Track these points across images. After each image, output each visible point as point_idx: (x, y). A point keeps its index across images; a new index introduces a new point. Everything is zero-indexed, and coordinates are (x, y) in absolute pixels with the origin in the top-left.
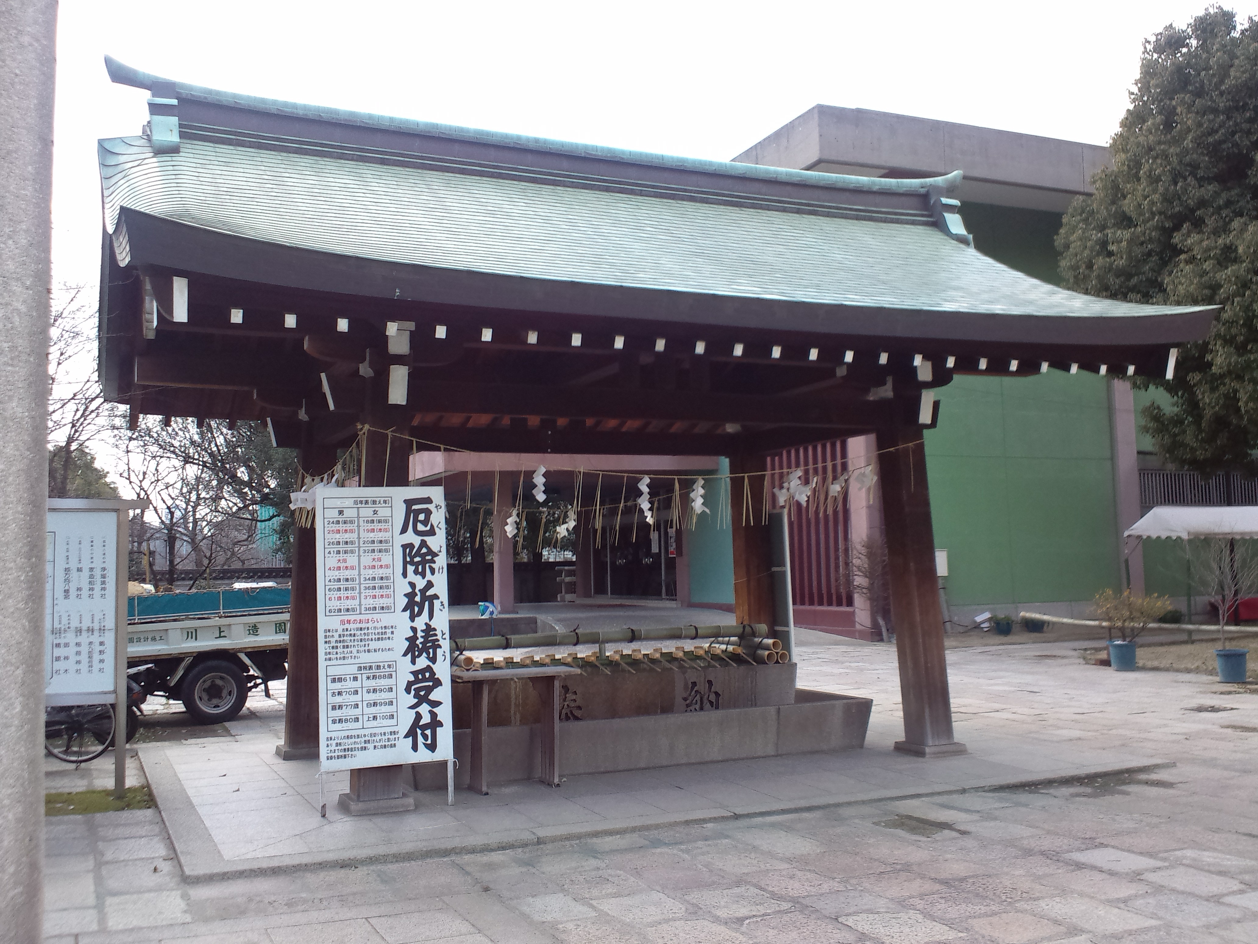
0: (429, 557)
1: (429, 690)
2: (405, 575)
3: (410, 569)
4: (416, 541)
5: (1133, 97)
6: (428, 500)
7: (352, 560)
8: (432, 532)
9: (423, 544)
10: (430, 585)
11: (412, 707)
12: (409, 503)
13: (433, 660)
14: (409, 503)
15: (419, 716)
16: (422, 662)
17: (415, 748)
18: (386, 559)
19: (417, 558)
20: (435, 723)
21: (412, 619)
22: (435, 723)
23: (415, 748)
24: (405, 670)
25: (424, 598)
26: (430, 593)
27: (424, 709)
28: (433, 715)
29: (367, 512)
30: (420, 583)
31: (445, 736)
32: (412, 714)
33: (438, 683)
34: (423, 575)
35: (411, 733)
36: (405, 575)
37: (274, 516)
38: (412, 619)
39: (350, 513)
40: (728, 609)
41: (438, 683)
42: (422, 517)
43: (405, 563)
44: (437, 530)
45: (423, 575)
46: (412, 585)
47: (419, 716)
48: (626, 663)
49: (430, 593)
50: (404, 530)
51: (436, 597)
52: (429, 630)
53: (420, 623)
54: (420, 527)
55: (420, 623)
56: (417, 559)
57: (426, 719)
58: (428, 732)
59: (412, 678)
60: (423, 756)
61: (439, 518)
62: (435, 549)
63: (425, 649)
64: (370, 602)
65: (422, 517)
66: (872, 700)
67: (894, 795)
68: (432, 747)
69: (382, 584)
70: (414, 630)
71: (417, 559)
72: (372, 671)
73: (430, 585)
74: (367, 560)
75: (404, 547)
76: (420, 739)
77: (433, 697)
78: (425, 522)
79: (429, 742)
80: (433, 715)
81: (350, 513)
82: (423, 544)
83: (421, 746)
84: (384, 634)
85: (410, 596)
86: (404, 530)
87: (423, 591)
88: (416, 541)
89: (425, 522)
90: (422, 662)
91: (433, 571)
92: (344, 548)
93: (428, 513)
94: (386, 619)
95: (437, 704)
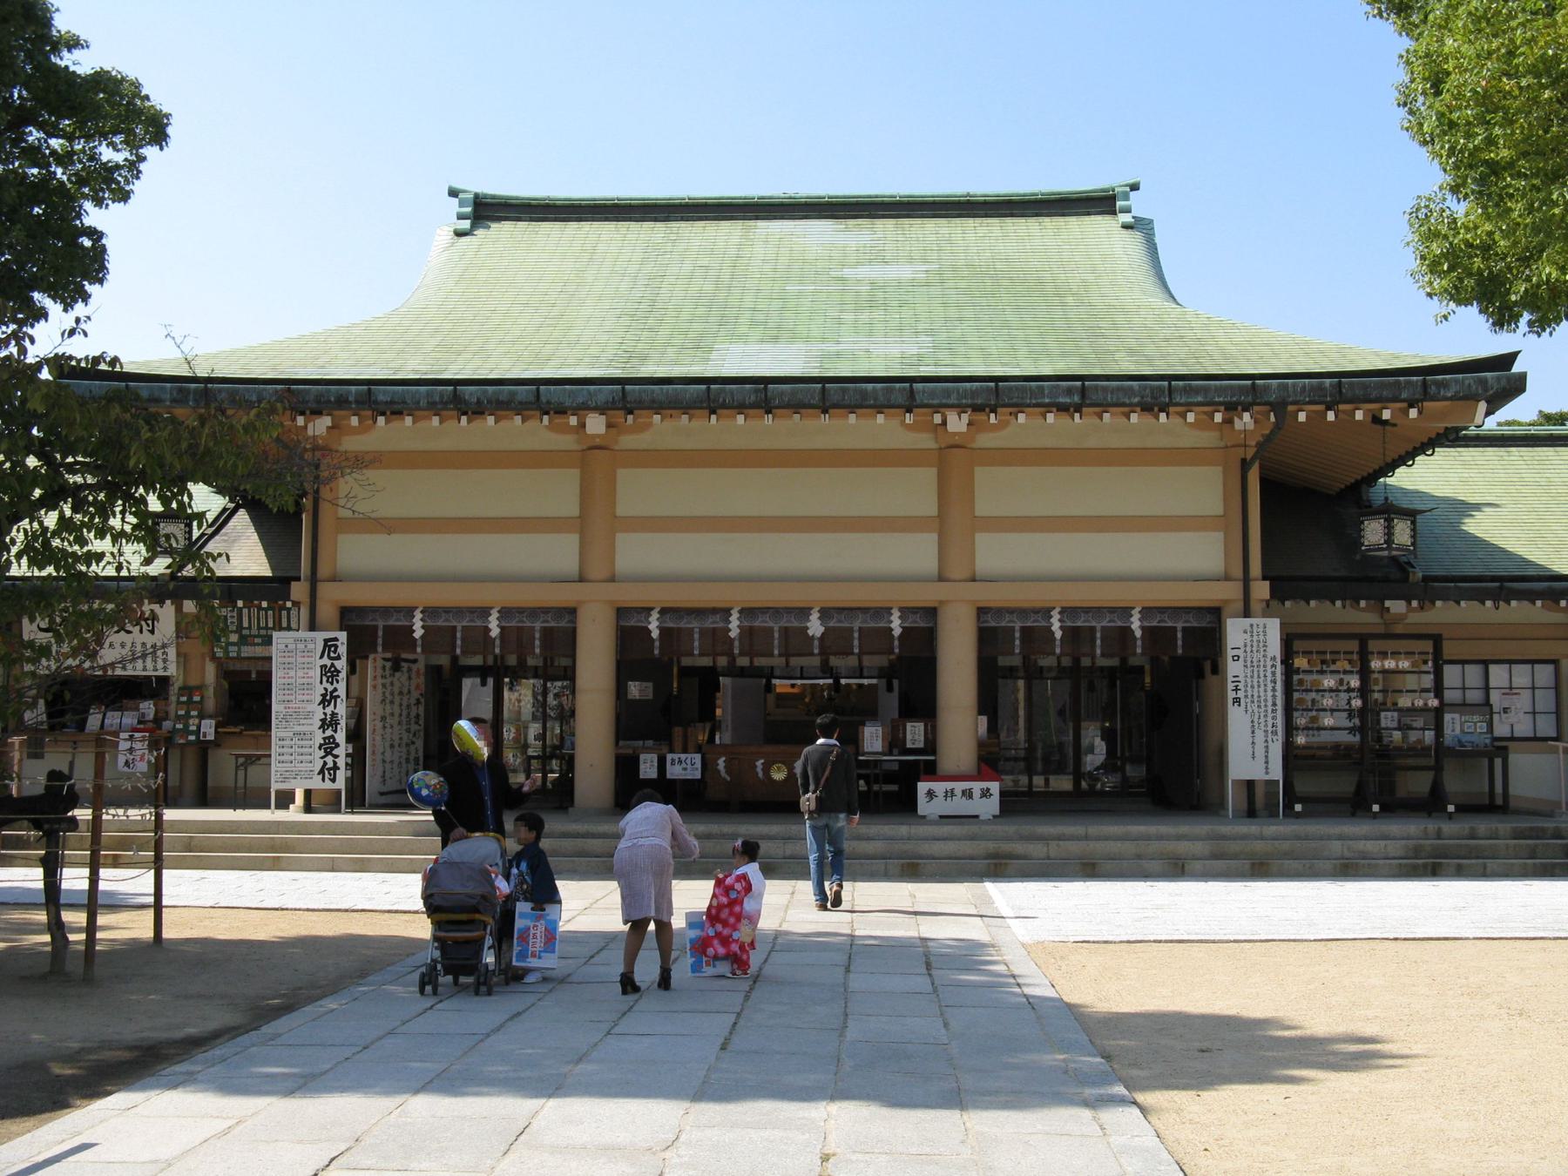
4: (328, 663)
5: (1436, 248)
6: (336, 639)
7: (292, 673)
8: (338, 658)
12: (326, 641)
14: (326, 641)
16: (329, 733)
18: (311, 673)
20: (335, 768)
24: (319, 738)
27: (329, 759)
29: (301, 646)
30: (330, 688)
31: (342, 775)
32: (321, 763)
33: (337, 745)
35: (321, 772)
37: (1008, 759)
39: (291, 647)
40: (556, 854)
41: (337, 745)
52: (333, 714)
53: (329, 710)
55: (329, 710)
57: (330, 764)
60: (328, 785)
61: (342, 650)
63: (330, 725)
64: (300, 697)
66: (101, 281)
68: (333, 780)
69: (309, 687)
72: (301, 735)
74: (300, 673)
81: (291, 647)
84: (309, 715)
85: (324, 696)
88: (328, 663)
90: (329, 733)
92: (287, 666)
94: (310, 707)
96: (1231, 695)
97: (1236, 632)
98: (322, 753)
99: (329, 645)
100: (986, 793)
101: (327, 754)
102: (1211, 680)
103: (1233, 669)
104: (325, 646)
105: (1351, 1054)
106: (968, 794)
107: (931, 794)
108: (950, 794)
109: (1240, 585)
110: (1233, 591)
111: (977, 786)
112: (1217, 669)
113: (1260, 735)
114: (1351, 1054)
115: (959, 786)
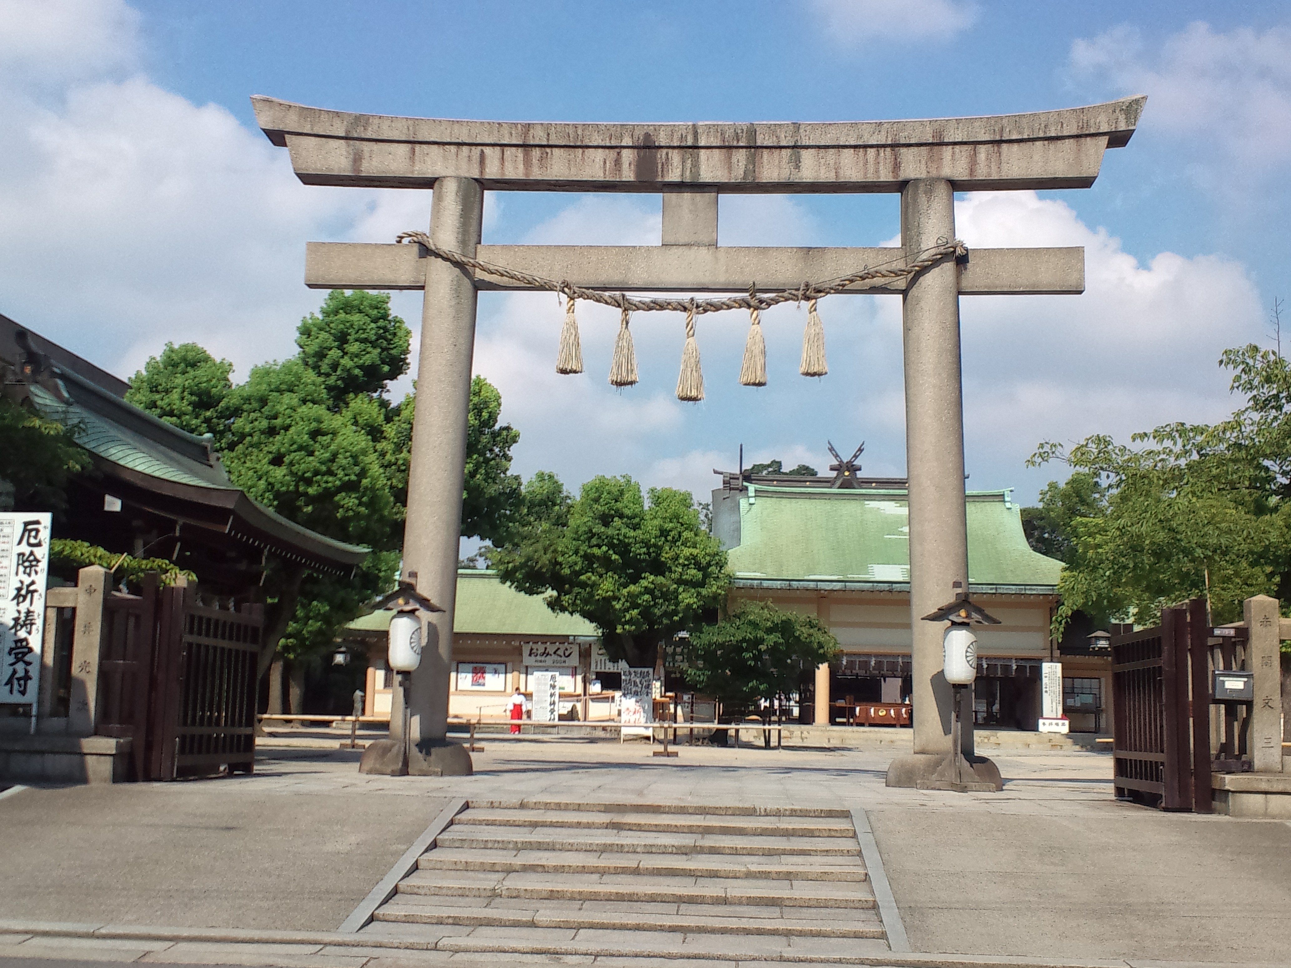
0: (34, 563)
1: (25, 654)
2: (17, 574)
3: (21, 569)
4: (26, 550)
6: (37, 522)
8: (39, 545)
9: (32, 553)
10: (33, 583)
11: (12, 664)
12: (26, 524)
13: (29, 633)
14: (26, 524)
15: (15, 672)
17: (11, 692)
18: (5, 562)
19: (27, 562)
20: (27, 678)
21: (18, 604)
22: (27, 678)
23: (11, 692)
25: (28, 592)
26: (32, 588)
27: (20, 667)
28: (27, 671)
32: (10, 671)
34: (29, 575)
35: (9, 682)
36: (17, 574)
38: (18, 604)
42: (33, 533)
43: (18, 565)
44: (43, 543)
45: (29, 575)
46: (22, 582)
47: (15, 672)
48: (839, 488)
49: (32, 588)
50: (20, 543)
51: (35, 591)
52: (29, 613)
53: (24, 607)
54: (32, 541)
55: (24, 607)
56: (27, 564)
57: (21, 673)
58: (22, 682)
59: (13, 645)
60: (17, 698)
61: (45, 534)
62: (39, 557)
63: (25, 625)
65: (33, 533)
67: (294, 946)
68: (23, 693)
70: (19, 612)
71: (27, 564)
73: (33, 583)
75: (19, 555)
76: (16, 686)
77: (27, 658)
78: (35, 537)
79: (22, 689)
80: (27, 671)
82: (32, 553)
83: (15, 692)
85: (19, 589)
86: (20, 543)
87: (28, 586)
89: (35, 537)
91: (36, 572)
93: (37, 531)
95: (28, 664)
96: (1044, 690)
97: (1046, 667)
98: (12, 659)
99: (29, 529)
100: (1063, 724)
101: (18, 660)
102: (1039, 682)
103: (1045, 681)
104: (25, 530)
105: (923, 619)
106: (1057, 724)
107: (1044, 724)
108: (1051, 724)
109: (1049, 652)
110: (1047, 653)
111: (1060, 722)
112: (1041, 679)
113: (1054, 704)
114: (923, 619)
115: (1054, 722)
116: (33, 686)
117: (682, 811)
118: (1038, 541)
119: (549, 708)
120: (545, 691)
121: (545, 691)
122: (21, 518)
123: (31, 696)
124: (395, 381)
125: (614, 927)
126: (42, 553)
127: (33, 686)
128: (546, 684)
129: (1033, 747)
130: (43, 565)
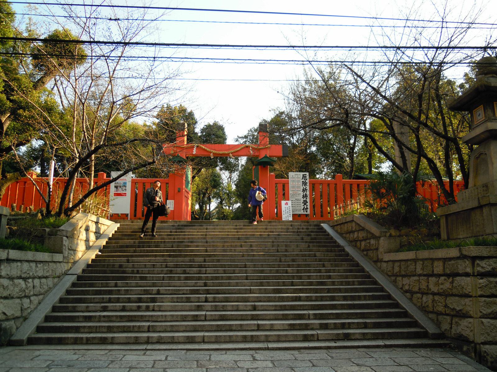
12: (303, 175)
19: (304, 183)
20: (307, 208)
22: (307, 208)
27: (305, 206)
35: (303, 209)
52: (306, 194)
60: (305, 213)
61: (308, 177)
68: (307, 212)
85: (303, 189)
99: (304, 177)
116: (309, 210)
117: (89, 341)
118: (48, 165)
119: (302, 200)
120: (299, 187)
121: (299, 187)
122: (302, 173)
123: (309, 212)
124: (197, 116)
125: (99, 350)
126: (307, 181)
127: (309, 210)
128: (298, 181)
129: (286, 206)
130: (308, 184)
